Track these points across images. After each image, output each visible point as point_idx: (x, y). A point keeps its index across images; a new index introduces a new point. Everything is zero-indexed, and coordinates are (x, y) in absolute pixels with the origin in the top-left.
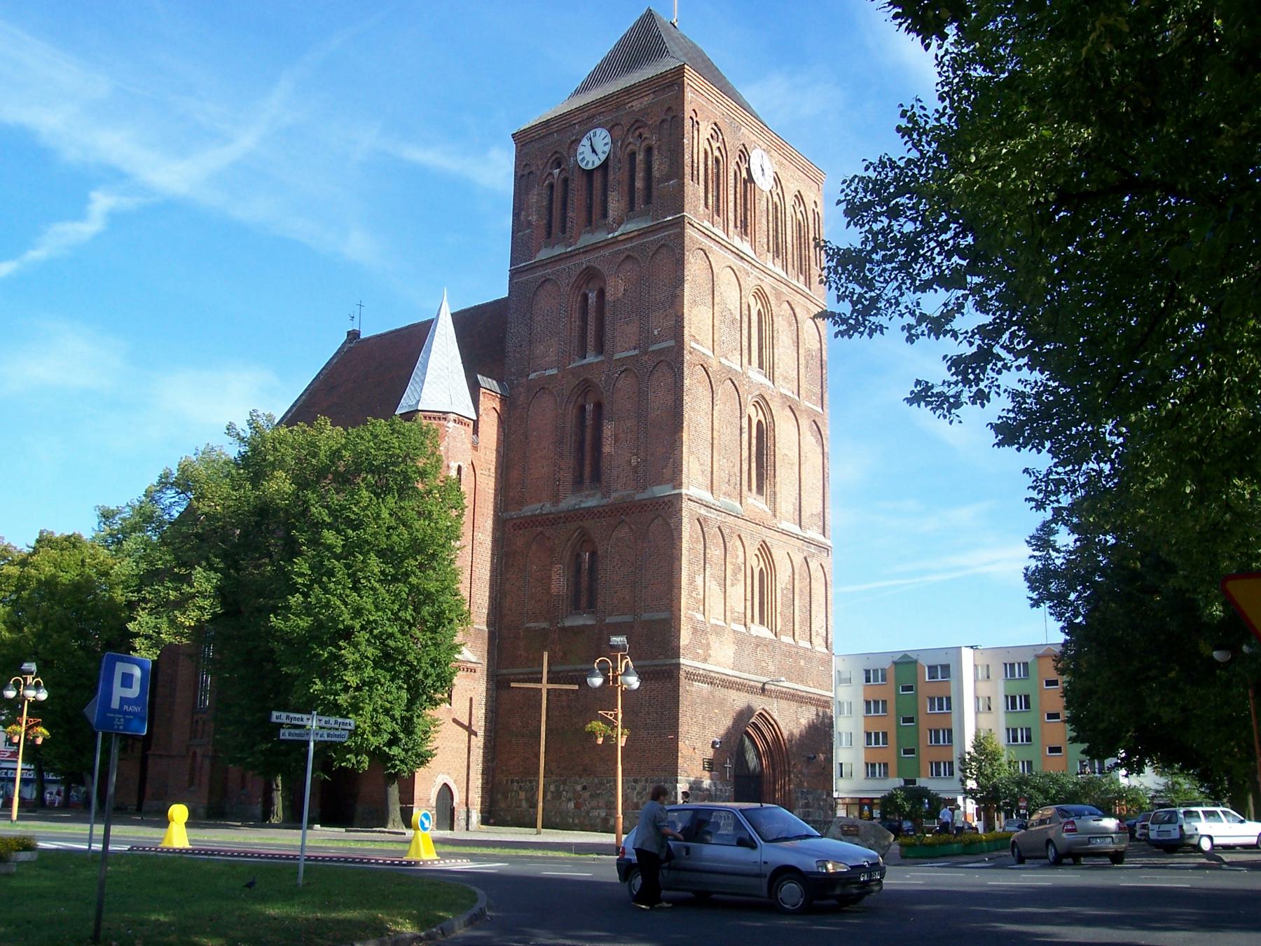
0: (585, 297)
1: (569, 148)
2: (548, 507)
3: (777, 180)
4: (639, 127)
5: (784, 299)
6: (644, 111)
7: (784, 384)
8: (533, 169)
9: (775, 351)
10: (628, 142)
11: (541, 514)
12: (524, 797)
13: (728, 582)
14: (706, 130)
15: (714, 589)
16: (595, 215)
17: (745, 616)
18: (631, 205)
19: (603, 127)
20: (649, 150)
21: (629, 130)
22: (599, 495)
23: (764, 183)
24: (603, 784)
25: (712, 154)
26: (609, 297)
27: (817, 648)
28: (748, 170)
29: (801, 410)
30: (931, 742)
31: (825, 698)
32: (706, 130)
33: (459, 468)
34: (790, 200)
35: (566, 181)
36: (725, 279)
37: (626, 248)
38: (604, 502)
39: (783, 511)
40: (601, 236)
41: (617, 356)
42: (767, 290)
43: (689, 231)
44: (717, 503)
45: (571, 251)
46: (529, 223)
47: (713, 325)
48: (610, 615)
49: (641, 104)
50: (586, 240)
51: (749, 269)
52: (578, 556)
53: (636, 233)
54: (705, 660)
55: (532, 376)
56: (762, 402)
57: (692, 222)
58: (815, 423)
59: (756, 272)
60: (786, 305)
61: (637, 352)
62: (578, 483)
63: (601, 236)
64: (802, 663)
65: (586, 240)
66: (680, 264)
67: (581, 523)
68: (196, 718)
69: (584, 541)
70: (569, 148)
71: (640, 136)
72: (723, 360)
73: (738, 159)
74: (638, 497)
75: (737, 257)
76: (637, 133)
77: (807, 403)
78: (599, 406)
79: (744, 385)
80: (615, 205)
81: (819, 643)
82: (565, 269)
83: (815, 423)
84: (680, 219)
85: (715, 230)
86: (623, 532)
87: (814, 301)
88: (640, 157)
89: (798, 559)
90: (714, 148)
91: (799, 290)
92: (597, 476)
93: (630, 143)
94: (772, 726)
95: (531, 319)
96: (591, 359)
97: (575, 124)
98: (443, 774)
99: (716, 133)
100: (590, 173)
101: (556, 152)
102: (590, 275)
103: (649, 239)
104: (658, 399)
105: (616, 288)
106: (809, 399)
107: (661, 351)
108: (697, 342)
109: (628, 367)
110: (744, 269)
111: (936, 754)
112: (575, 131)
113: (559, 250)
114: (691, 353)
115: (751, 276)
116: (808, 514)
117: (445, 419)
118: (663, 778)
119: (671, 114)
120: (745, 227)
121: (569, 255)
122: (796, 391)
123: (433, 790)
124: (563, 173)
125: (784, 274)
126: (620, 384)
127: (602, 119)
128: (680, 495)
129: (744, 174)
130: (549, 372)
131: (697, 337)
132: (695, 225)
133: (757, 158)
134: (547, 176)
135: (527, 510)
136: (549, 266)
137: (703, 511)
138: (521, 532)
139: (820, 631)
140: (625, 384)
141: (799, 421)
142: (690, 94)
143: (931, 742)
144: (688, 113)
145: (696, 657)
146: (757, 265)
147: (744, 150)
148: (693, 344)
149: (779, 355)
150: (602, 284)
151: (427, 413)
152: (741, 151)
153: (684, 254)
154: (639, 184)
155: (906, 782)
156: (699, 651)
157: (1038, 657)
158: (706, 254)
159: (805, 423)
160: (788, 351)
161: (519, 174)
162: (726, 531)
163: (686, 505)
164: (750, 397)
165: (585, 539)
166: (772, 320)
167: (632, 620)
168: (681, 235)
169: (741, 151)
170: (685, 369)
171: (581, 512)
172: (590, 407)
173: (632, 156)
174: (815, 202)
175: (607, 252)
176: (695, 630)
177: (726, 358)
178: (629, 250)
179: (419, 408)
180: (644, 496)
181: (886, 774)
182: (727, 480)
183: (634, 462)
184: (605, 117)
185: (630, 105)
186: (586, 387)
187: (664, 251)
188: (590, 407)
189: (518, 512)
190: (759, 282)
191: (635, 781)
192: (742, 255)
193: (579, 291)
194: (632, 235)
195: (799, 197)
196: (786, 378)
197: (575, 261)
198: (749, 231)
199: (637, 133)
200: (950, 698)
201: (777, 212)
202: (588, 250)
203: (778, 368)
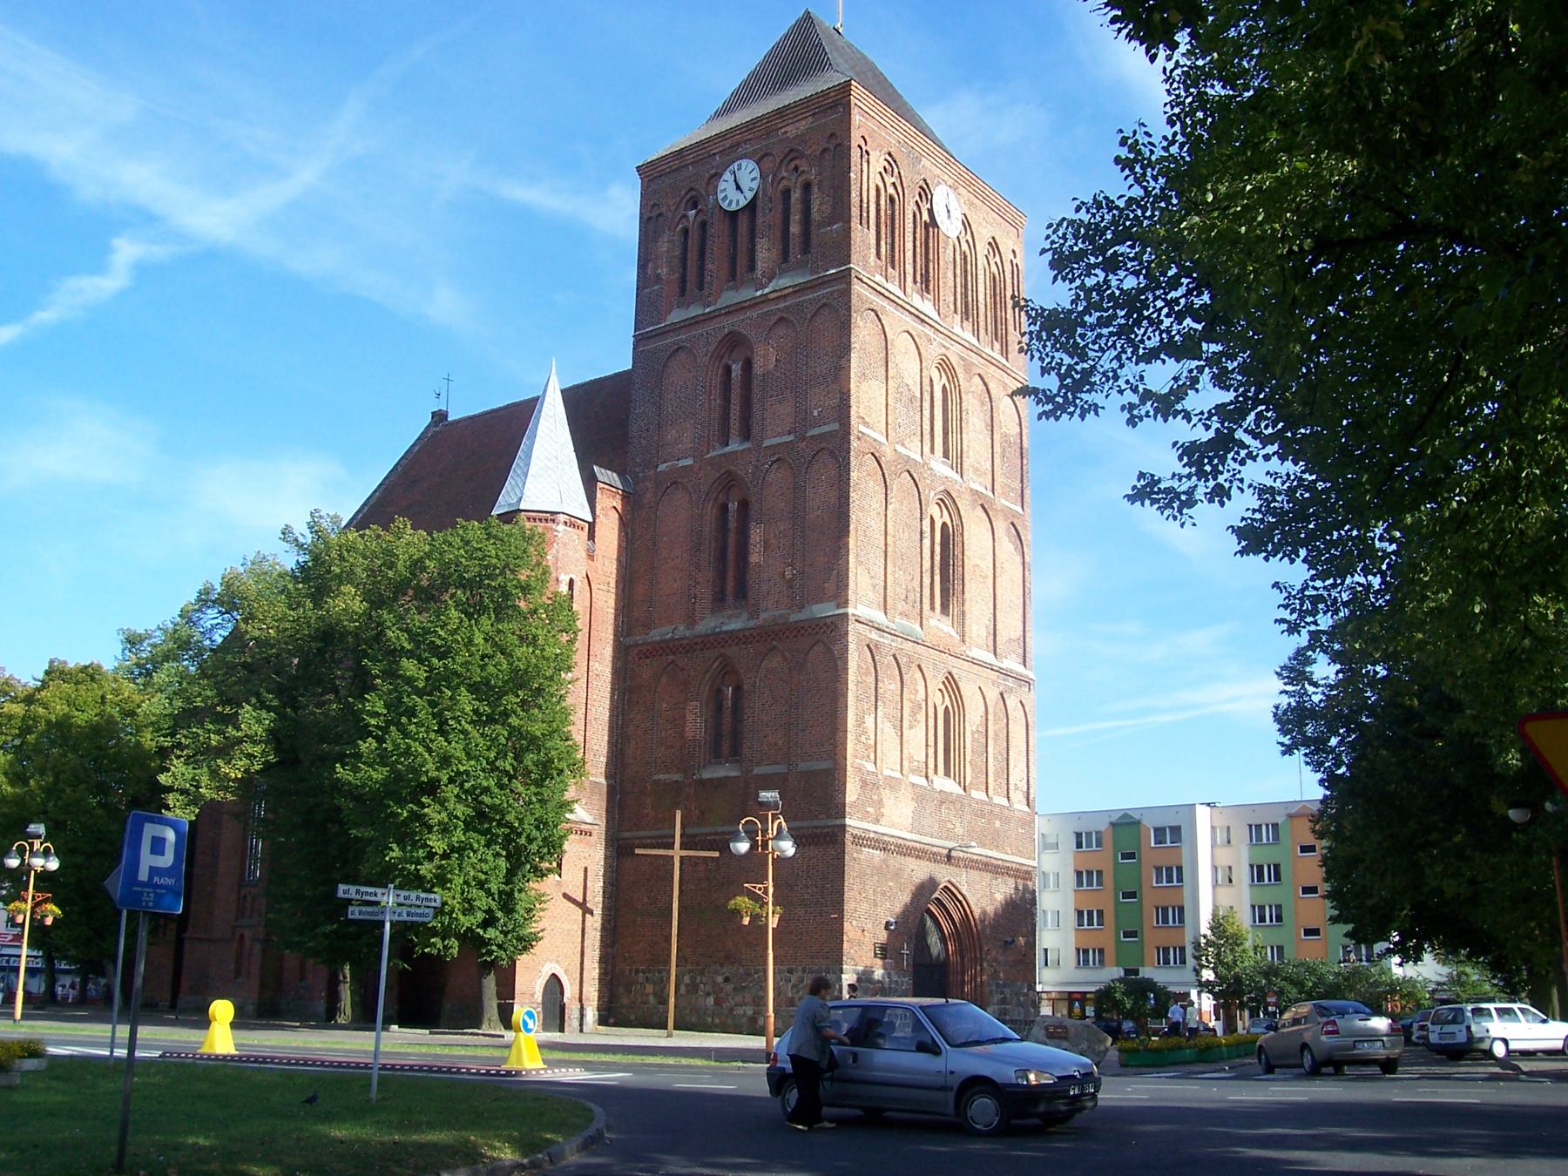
0: (728, 370)
1: (708, 184)
2: (682, 630)
3: (966, 224)
4: (795, 158)
5: (974, 372)
6: (801, 139)
7: (975, 478)
8: (663, 210)
9: (964, 436)
10: (781, 176)
11: (672, 639)
12: (651, 991)
13: (906, 724)
14: (878, 162)
15: (888, 732)
16: (740, 268)
17: (927, 765)
18: (785, 254)
19: (750, 158)
20: (807, 187)
21: (782, 161)
22: (745, 616)
23: (950, 227)
24: (750, 975)
25: (886, 191)
26: (758, 369)
27: (1016, 806)
28: (931, 212)
29: (996, 510)
30: (1158, 923)
31: (1026, 868)
32: (878, 162)
33: (571, 582)
34: (982, 249)
35: (703, 225)
36: (902, 346)
37: (779, 309)
38: (752, 624)
39: (974, 635)
40: (747, 294)
41: (767, 443)
42: (954, 361)
43: (857, 287)
44: (892, 625)
45: (710, 312)
46: (658, 278)
47: (887, 405)
48: (759, 764)
49: (797, 129)
50: (729, 298)
51: (931, 334)
52: (719, 691)
53: (791, 290)
54: (877, 821)
55: (662, 467)
56: (947, 500)
57: (861, 277)
58: (1014, 526)
59: (940, 339)
60: (977, 380)
61: (791, 437)
62: (719, 600)
63: (747, 294)
64: (998, 824)
65: (729, 298)
66: (845, 328)
67: (722, 651)
68: (243, 892)
69: (725, 673)
70: (708, 184)
71: (796, 168)
72: (899, 448)
73: (917, 198)
74: (794, 617)
75: (916, 319)
76: (792, 165)
77: (1003, 501)
78: (744, 505)
79: (925, 478)
80: (765, 254)
81: (1018, 799)
82: (702, 335)
83: (1014, 526)
84: (846, 272)
85: (889, 286)
86: (774, 662)
87: (1013, 374)
88: (796, 195)
89: (992, 695)
90: (888, 184)
91: (993, 361)
92: (742, 592)
93: (783, 178)
94: (960, 902)
95: (660, 396)
96: (734, 446)
97: (714, 154)
98: (551, 961)
99: (891, 165)
100: (733, 216)
101: (692, 189)
102: (734, 342)
103: (807, 297)
104: (818, 496)
105: (766, 358)
106: (1005, 495)
107: (822, 437)
108: (866, 424)
109: (780, 456)
110: (926, 335)
111: (1163, 938)
112: (714, 164)
113: (695, 311)
114: (859, 439)
115: (934, 343)
116: (1005, 639)
117: (553, 521)
118: (824, 967)
119: (834, 142)
120: (926, 282)
121: (707, 317)
122: (989, 487)
123: (539, 982)
124: (701, 214)
125: (974, 341)
126: (771, 477)
127: (749, 148)
128: (846, 615)
129: (926, 217)
130: (682, 463)
131: (867, 419)
132: (865, 280)
133: (942, 197)
134: (681, 219)
135: (656, 635)
136: (683, 331)
137: (874, 635)
138: (648, 661)
139: (1019, 784)
140: (777, 478)
141: (994, 523)
142: (858, 117)
143: (1158, 923)
144: (856, 140)
145: (865, 817)
146: (941, 329)
147: (925, 187)
148: (862, 428)
149: (969, 441)
150: (749, 353)
151: (530, 514)
152: (921, 187)
153: (850, 316)
154: (795, 229)
155: (1127, 972)
156: (869, 809)
157: (1291, 816)
158: (877, 316)
159: (1001, 526)
160: (980, 437)
161: (645, 217)
162: (903, 660)
163: (853, 628)
164: (932, 493)
165: (728, 671)
166: (961, 398)
167: (786, 771)
168: (847, 293)
169: (921, 187)
170: (852, 459)
171: (722, 636)
172: (733, 506)
173: (786, 193)
174: (1014, 251)
175: (754, 314)
176: (864, 784)
177: (903, 445)
178: (782, 311)
179: (521, 507)
180: (802, 616)
181: (1102, 962)
182: (904, 597)
183: (788, 575)
184: (752, 146)
185: (783, 130)
186: (729, 481)
187: (826, 311)
188: (733, 506)
189: (644, 636)
190: (943, 351)
191: (790, 971)
192: (922, 317)
193: (720, 362)
194: (786, 292)
195: (994, 245)
196: (977, 470)
197: (715, 324)
198: (931, 288)
199: (792, 165)
200: (1181, 867)
201: (966, 264)
202: (731, 311)
203: (968, 457)
